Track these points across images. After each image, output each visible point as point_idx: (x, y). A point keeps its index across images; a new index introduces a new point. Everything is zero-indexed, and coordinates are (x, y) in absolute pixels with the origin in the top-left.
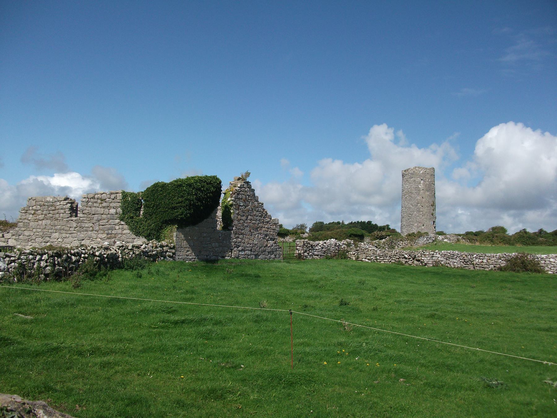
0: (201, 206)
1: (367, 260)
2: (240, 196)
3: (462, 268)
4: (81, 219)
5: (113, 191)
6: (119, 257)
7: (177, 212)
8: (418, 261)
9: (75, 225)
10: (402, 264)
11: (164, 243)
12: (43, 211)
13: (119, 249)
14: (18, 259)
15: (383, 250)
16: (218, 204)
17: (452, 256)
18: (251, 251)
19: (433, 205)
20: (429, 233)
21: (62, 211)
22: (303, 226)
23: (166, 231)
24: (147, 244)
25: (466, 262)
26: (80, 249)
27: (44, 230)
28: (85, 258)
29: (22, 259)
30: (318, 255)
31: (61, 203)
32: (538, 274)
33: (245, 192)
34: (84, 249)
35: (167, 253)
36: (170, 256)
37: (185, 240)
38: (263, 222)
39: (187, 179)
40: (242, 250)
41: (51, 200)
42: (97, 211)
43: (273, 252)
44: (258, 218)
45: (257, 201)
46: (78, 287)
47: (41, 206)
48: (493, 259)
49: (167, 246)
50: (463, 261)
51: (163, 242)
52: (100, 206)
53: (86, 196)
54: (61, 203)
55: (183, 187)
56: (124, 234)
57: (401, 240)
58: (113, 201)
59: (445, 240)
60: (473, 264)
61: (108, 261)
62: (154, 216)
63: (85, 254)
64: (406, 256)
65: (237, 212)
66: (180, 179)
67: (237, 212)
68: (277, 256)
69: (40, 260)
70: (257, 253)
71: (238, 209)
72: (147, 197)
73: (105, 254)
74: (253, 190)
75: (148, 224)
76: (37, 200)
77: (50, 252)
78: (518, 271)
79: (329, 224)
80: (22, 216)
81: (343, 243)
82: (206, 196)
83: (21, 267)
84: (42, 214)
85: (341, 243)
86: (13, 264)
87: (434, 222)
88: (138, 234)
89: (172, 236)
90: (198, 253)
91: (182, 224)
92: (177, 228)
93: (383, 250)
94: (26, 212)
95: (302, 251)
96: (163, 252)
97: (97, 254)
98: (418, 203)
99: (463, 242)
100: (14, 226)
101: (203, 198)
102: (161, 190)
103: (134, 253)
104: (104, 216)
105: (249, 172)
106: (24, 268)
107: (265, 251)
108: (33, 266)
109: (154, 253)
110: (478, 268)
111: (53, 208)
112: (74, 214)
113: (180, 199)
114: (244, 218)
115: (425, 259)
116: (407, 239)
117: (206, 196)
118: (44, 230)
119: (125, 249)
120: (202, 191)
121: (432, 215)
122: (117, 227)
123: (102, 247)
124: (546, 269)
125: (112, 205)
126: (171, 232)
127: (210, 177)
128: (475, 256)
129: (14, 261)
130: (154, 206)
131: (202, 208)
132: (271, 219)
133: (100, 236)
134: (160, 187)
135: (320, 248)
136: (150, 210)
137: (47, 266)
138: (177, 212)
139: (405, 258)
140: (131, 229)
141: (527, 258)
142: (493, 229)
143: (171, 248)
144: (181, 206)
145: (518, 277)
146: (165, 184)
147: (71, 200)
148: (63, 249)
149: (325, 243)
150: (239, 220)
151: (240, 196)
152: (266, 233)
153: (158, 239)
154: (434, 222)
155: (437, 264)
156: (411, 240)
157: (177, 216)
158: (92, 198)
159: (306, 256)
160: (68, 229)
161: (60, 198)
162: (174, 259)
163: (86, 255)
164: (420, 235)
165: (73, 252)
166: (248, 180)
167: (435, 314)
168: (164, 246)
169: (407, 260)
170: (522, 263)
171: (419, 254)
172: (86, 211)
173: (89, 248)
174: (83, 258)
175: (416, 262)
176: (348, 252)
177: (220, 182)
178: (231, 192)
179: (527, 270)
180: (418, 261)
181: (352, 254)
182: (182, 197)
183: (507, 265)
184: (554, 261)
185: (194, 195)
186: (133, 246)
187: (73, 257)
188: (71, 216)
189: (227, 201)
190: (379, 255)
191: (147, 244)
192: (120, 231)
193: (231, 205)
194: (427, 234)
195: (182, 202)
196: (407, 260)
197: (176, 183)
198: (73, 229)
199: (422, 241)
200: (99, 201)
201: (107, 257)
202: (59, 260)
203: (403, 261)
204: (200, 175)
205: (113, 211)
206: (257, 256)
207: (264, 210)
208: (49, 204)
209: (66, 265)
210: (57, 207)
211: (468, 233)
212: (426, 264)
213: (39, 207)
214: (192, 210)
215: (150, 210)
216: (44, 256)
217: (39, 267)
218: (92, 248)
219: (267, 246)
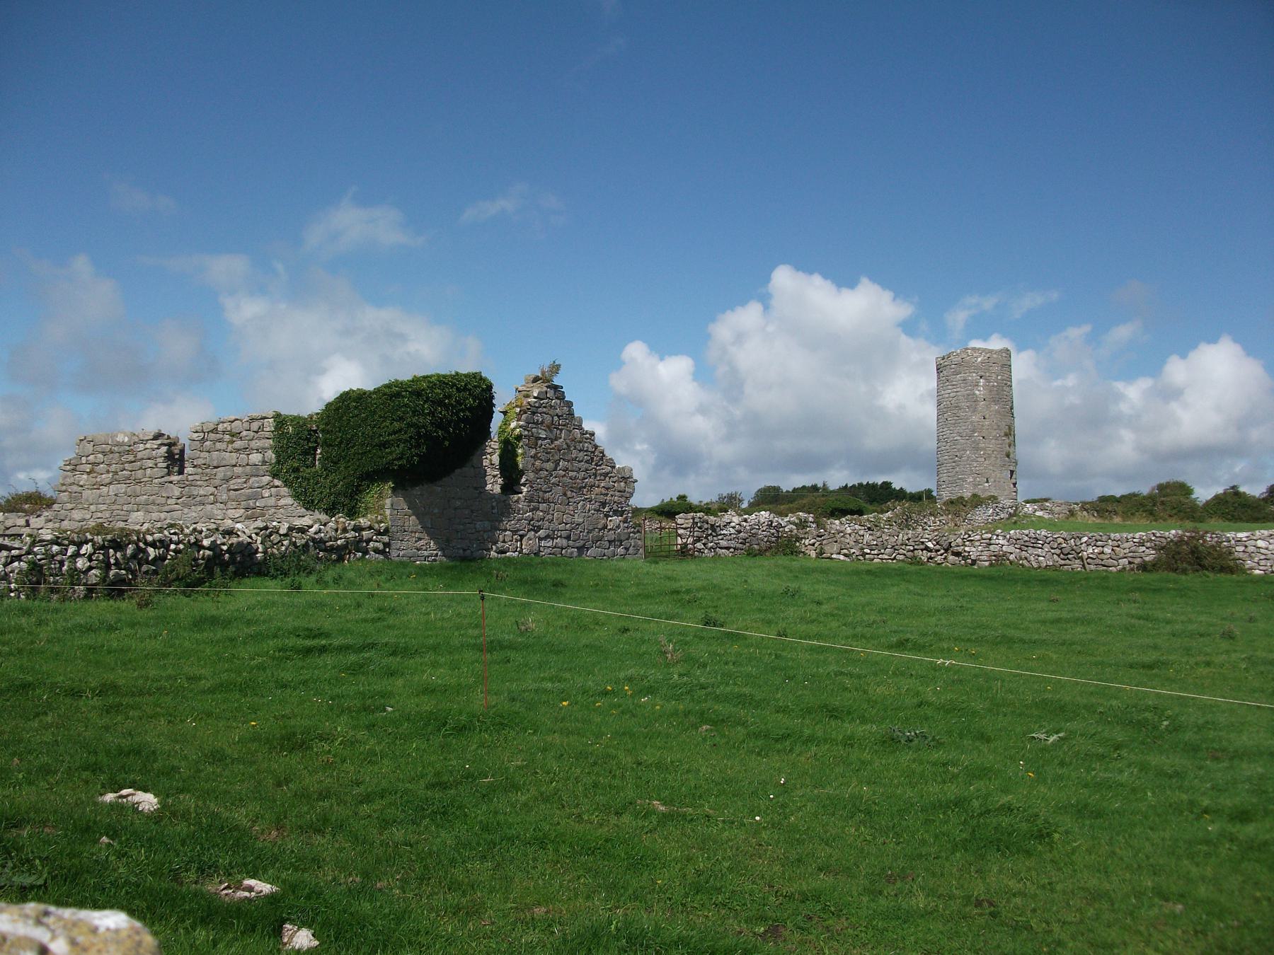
0: (444, 438)
1: (842, 557)
2: (538, 418)
3: (1055, 568)
4: (190, 478)
5: (255, 414)
6: (257, 551)
7: (391, 453)
8: (957, 554)
9: (177, 491)
10: (920, 563)
11: (363, 521)
12: (109, 465)
14: (28, 553)
15: (878, 534)
16: (486, 434)
17: (1034, 542)
18: (568, 538)
19: (1010, 433)
20: (1000, 498)
21: (150, 463)
22: (735, 498)
23: (370, 497)
24: (325, 525)
25: (1064, 554)
26: (166, 532)
28: (177, 551)
29: (36, 554)
30: (728, 548)
31: (148, 446)
32: (1229, 576)
33: (550, 407)
35: (371, 544)
36: (376, 551)
38: (595, 475)
40: (547, 537)
41: (126, 439)
43: (621, 541)
44: (583, 465)
46: (147, 605)
48: (1126, 545)
49: (370, 528)
50: (1058, 551)
53: (199, 428)
54: (148, 446)
56: (282, 507)
57: (931, 514)
59: (1038, 514)
60: (1081, 558)
62: (342, 466)
63: (177, 544)
64: (930, 545)
65: (533, 452)
67: (533, 452)
69: (77, 555)
72: (327, 424)
74: (570, 404)
77: (99, 539)
78: (1184, 571)
79: (795, 490)
80: (65, 477)
81: (787, 522)
82: (455, 418)
83: (33, 569)
84: (108, 472)
85: (783, 521)
86: (16, 564)
87: (1012, 472)
88: (310, 505)
89: (382, 507)
92: (394, 490)
94: (75, 470)
95: (691, 540)
97: (206, 543)
98: (974, 431)
99: (1083, 516)
100: (50, 503)
101: (449, 422)
102: (356, 407)
104: (238, 470)
106: (41, 572)
108: (60, 568)
109: (339, 542)
110: (1092, 567)
111: (131, 458)
112: (176, 469)
114: (549, 466)
115: (973, 551)
116: (947, 512)
117: (455, 418)
119: (271, 534)
121: (1008, 456)
124: (1249, 563)
125: (254, 444)
126: (381, 497)
127: (466, 376)
128: (1085, 539)
129: (18, 558)
130: (341, 443)
131: (447, 443)
133: (231, 513)
135: (732, 531)
137: (91, 568)
138: (391, 453)
139: (927, 549)
140: (296, 496)
141: (1205, 541)
142: (1161, 487)
143: (379, 533)
145: (1176, 582)
146: (365, 393)
147: (169, 438)
151: (538, 418)
152: (602, 498)
153: (352, 514)
154: (1012, 472)
155: (1000, 558)
156: (957, 514)
157: (391, 463)
158: (212, 431)
159: (699, 551)
160: (163, 501)
161: (145, 434)
162: (387, 557)
163: (181, 546)
164: (977, 501)
165: (149, 538)
166: (556, 381)
167: (907, 640)
168: (363, 529)
169: (933, 554)
170: (1192, 552)
171: (959, 540)
172: (200, 462)
173: (187, 531)
174: (174, 551)
175: (951, 558)
176: (799, 539)
177: (490, 387)
178: (518, 410)
179: (1203, 567)
180: (957, 554)
181: (808, 544)
182: (401, 419)
183: (1159, 559)
184: (1264, 548)
186: (291, 529)
187: (151, 550)
188: (169, 474)
189: (509, 430)
190: (869, 545)
191: (325, 525)
192: (272, 501)
193: (519, 438)
194: (994, 499)
195: (400, 430)
196: (933, 554)
197: (387, 390)
198: (174, 501)
199: (981, 515)
200: (227, 437)
201: (228, 551)
202: (119, 555)
203: (924, 556)
204: (443, 373)
206: (581, 549)
207: (596, 447)
210: (140, 455)
211: (1103, 499)
212: (974, 562)
214: (424, 445)
217: (74, 571)
218: (195, 530)
219: (605, 527)
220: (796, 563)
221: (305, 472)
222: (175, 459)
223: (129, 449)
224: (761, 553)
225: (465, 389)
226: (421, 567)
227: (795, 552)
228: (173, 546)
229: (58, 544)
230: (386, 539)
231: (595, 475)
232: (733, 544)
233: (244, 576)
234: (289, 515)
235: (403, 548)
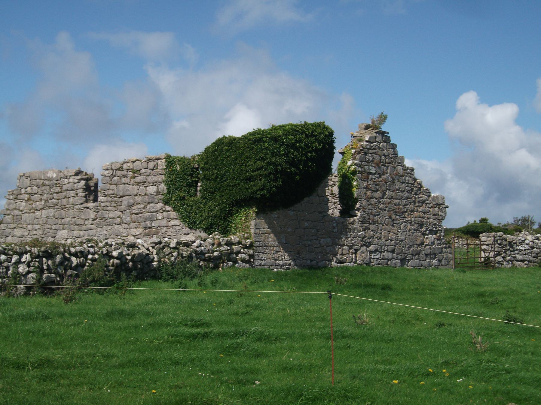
0: (296, 174)
2: (369, 157)
4: (103, 204)
5: (151, 156)
6: (153, 260)
7: (255, 185)
9: (92, 215)
11: (233, 238)
12: (42, 195)
13: (153, 247)
16: (328, 170)
18: (393, 251)
21: (72, 193)
22: (528, 221)
23: (239, 219)
24: (204, 240)
26: (85, 246)
27: (45, 227)
28: (93, 260)
30: (523, 261)
31: (71, 180)
33: (379, 148)
34: (92, 247)
35: (240, 256)
36: (243, 261)
37: (272, 232)
38: (415, 202)
39: (271, 130)
40: (376, 251)
41: (55, 175)
42: (127, 190)
43: (435, 254)
45: (402, 165)
46: (71, 300)
47: (38, 186)
51: (232, 237)
52: (132, 181)
53: (109, 167)
54: (71, 180)
55: (264, 142)
58: (152, 172)
61: (135, 267)
63: (93, 254)
65: (365, 184)
66: (259, 130)
67: (365, 184)
68: (443, 262)
69: (19, 262)
70: (404, 255)
71: (367, 179)
72: (206, 163)
73: (128, 255)
74: (394, 146)
75: (209, 207)
76: (33, 177)
80: (9, 204)
82: (304, 158)
84: (41, 200)
88: (193, 225)
89: (248, 227)
90: (296, 256)
91: (265, 205)
92: (257, 213)
94: (16, 198)
95: (492, 254)
96: (232, 253)
97: (115, 254)
101: (300, 161)
102: (228, 150)
103: (179, 254)
105: (384, 114)
107: (419, 253)
108: (7, 272)
109: (215, 254)
111: (58, 189)
112: (92, 198)
113: (259, 163)
114: (378, 195)
117: (304, 158)
118: (45, 227)
119: (163, 248)
120: (297, 149)
122: (160, 216)
123: (123, 244)
125: (150, 179)
126: (247, 219)
127: (313, 125)
130: (217, 177)
132: (429, 196)
134: (227, 146)
135: (527, 247)
136: (212, 184)
137: (29, 272)
138: (255, 185)
140: (182, 219)
143: (246, 247)
144: (261, 175)
147: (86, 174)
148: (55, 246)
150: (369, 199)
151: (369, 157)
152: (420, 220)
153: (225, 232)
157: (254, 193)
158: (119, 169)
159: (499, 263)
160: (82, 222)
163: (96, 256)
166: (384, 128)
172: (109, 192)
173: (101, 245)
177: (331, 134)
178: (353, 151)
182: (262, 159)
185: (284, 155)
186: (178, 243)
187: (74, 259)
188: (86, 202)
189: (346, 167)
191: (204, 240)
192: (164, 223)
193: (354, 173)
197: (251, 137)
198: (90, 222)
200: (130, 174)
201: (131, 260)
202: (50, 262)
205: (152, 189)
206: (403, 261)
207: (415, 180)
208: (51, 183)
209: (61, 270)
210: (65, 188)
213: (35, 188)
215: (212, 184)
216: (25, 256)
217: (17, 274)
218: (107, 244)
219: (422, 243)
221: (190, 200)
222: (91, 191)
223: (57, 183)
228: (90, 256)
230: (251, 252)
232: (527, 257)
234: (176, 232)
235: (263, 259)
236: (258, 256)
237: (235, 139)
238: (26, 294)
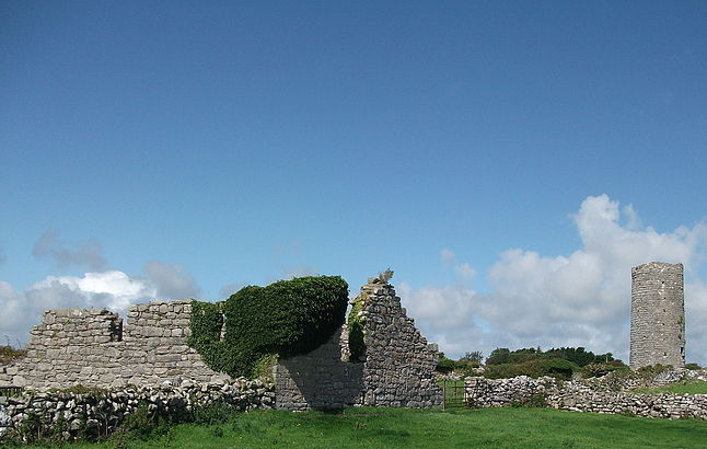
8: (658, 410)
11: (257, 382)
14: (29, 407)
15: (603, 393)
18: (395, 394)
19: (681, 322)
23: (262, 364)
29: (34, 408)
33: (386, 301)
36: (266, 403)
38: (414, 350)
49: (263, 386)
61: (171, 411)
62: (242, 340)
69: (63, 408)
72: (231, 310)
77: (79, 396)
84: (66, 337)
88: (217, 368)
89: (271, 372)
91: (286, 352)
93: (603, 393)
97: (153, 399)
103: (210, 398)
114: (384, 343)
115: (669, 408)
129: (22, 410)
130: (241, 324)
137: (73, 418)
139: (636, 405)
140: (206, 361)
143: (268, 390)
149: (511, 382)
152: (417, 366)
153: (249, 375)
156: (647, 378)
159: (481, 403)
163: (136, 402)
164: (660, 369)
165: (114, 396)
172: (135, 332)
176: (546, 396)
177: (346, 287)
180: (658, 410)
181: (553, 400)
182: (286, 309)
186: (209, 387)
187: (115, 404)
192: (188, 363)
193: (364, 323)
194: (671, 367)
199: (663, 379)
200: (156, 316)
201: (168, 405)
202: (93, 408)
203: (634, 410)
212: (669, 416)
214: (302, 329)
220: (550, 414)
221: (214, 344)
222: (116, 330)
223: (83, 321)
224: (521, 405)
225: (331, 289)
226: (299, 416)
227: (544, 405)
228: (130, 402)
229: (52, 401)
230: (273, 394)
231: (414, 350)
232: (502, 398)
233: (178, 423)
234: (198, 377)
235: (284, 401)
236: (279, 398)
237: (257, 292)
238: (71, 440)
